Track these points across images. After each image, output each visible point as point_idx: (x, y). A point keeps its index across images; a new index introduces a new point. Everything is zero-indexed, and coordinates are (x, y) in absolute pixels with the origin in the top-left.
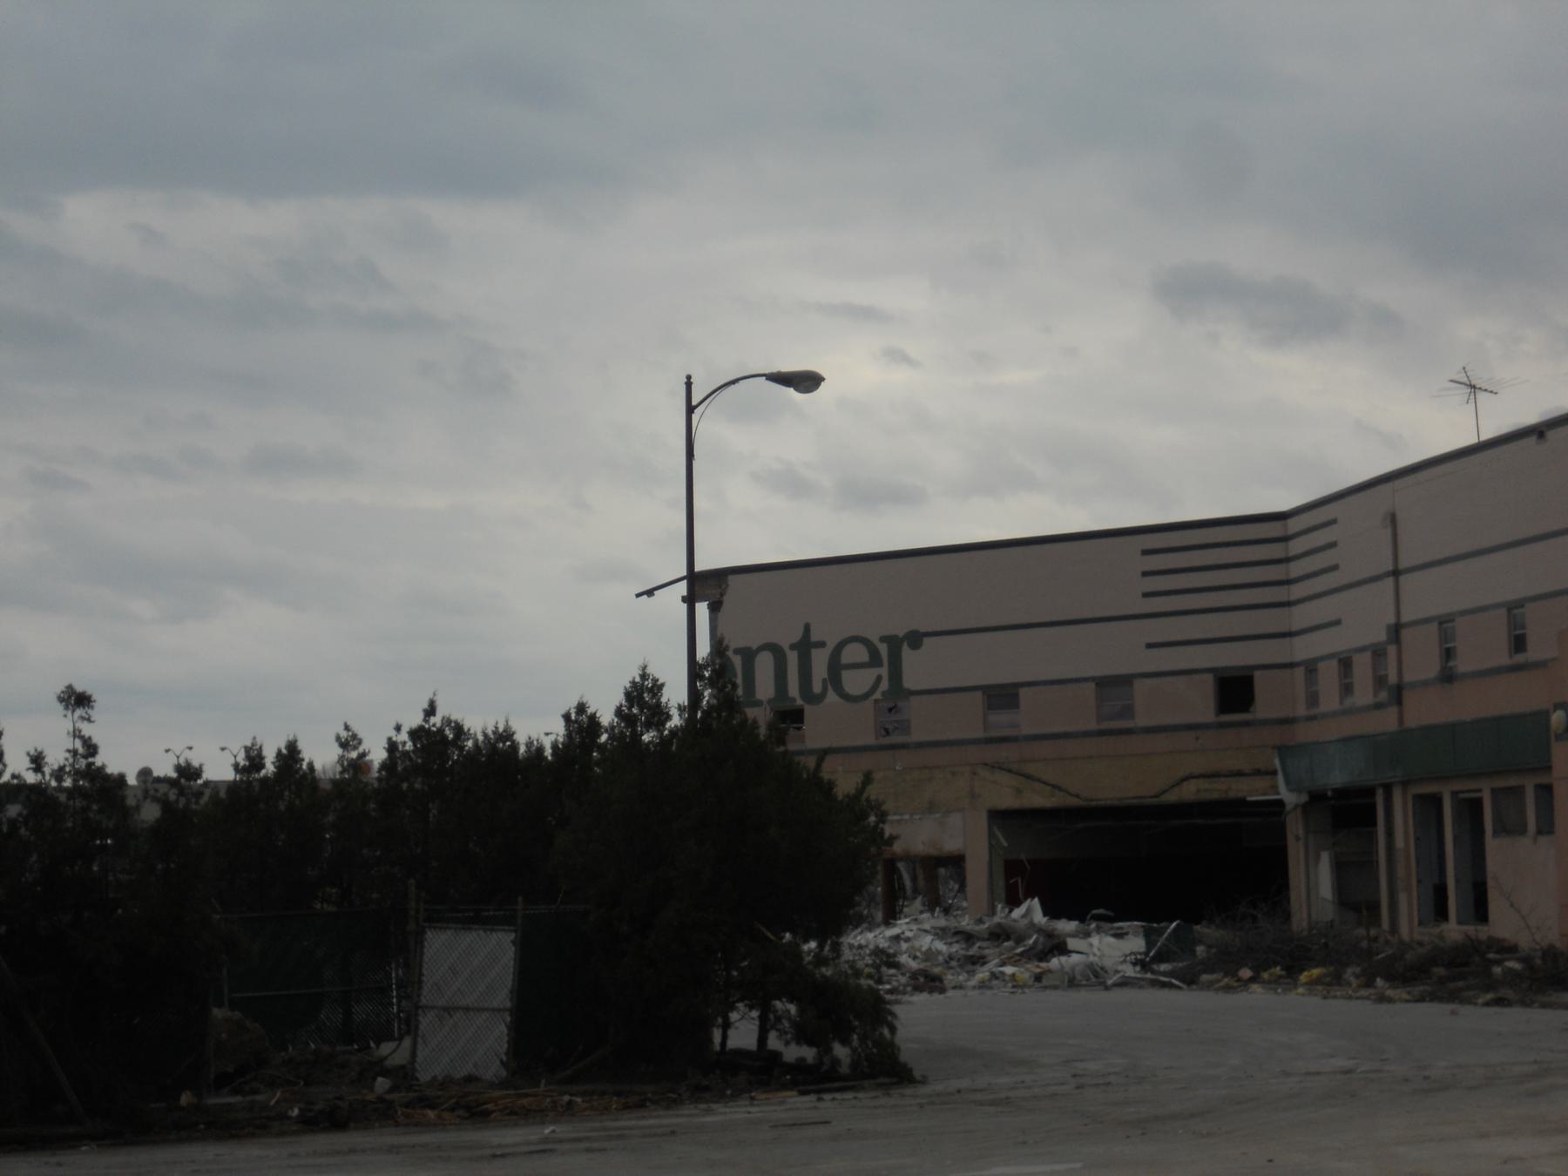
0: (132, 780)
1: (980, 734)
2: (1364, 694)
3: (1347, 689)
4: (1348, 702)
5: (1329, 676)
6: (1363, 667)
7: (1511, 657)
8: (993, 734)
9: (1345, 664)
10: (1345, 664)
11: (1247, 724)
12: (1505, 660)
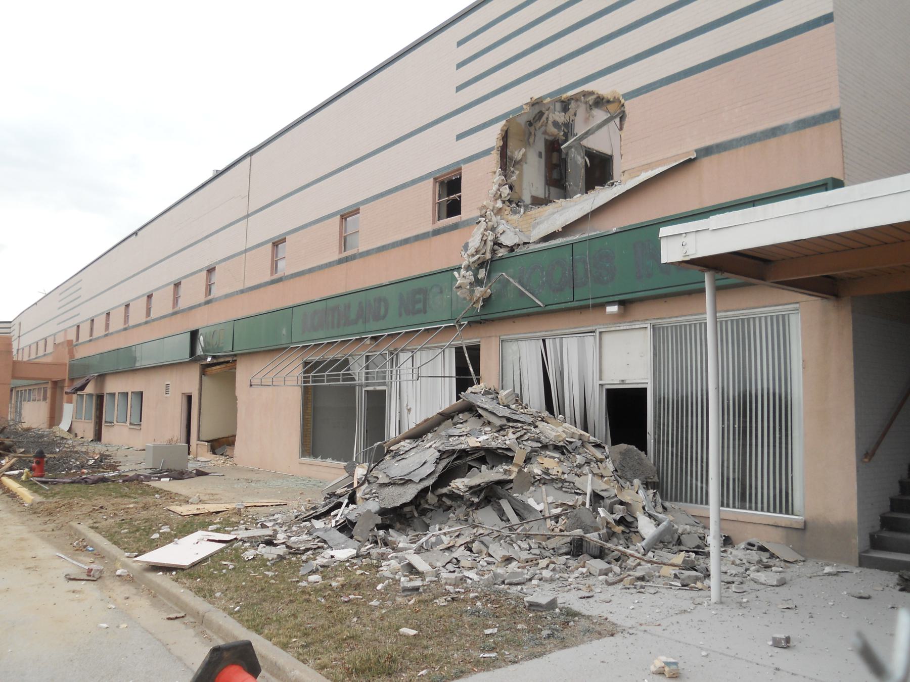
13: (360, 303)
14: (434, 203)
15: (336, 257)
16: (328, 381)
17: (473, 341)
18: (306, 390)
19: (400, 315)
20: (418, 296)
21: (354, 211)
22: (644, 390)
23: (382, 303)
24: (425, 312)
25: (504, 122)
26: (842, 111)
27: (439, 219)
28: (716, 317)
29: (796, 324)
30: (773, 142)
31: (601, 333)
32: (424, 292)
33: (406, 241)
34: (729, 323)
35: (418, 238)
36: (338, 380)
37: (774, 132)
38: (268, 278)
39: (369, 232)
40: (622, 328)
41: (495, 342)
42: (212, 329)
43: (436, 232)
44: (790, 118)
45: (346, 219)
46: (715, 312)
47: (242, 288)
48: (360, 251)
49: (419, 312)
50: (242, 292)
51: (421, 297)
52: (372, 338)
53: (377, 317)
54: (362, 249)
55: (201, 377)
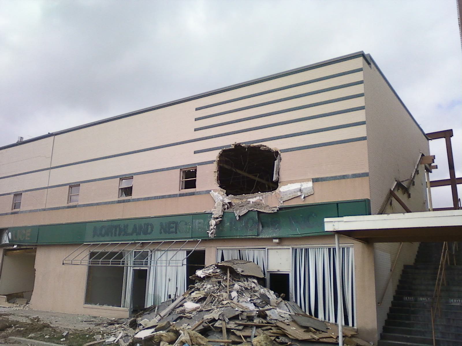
0: (143, 225)
13: (135, 225)
14: (180, 181)
15: (10, 211)
16: (112, 264)
17: (306, 246)
18: (90, 268)
19: (161, 233)
20: (172, 225)
21: (77, 185)
22: (288, 274)
23: (150, 226)
24: (176, 233)
25: (221, 150)
26: (370, 174)
27: (14, 209)
28: (339, 246)
29: (351, 250)
30: (343, 181)
31: (268, 249)
32: (176, 223)
33: (163, 197)
34: (300, 249)
35: (170, 196)
36: (109, 264)
37: (344, 177)
38: (66, 205)
39: (84, 196)
40: (278, 248)
41: (213, 250)
42: (110, 223)
43: (181, 195)
44: (350, 173)
45: (72, 188)
46: (339, 244)
47: (44, 207)
48: (79, 204)
49: (172, 232)
50: (44, 210)
51: (174, 225)
52: (142, 243)
53: (146, 233)
54: (80, 203)
55: (3, 256)
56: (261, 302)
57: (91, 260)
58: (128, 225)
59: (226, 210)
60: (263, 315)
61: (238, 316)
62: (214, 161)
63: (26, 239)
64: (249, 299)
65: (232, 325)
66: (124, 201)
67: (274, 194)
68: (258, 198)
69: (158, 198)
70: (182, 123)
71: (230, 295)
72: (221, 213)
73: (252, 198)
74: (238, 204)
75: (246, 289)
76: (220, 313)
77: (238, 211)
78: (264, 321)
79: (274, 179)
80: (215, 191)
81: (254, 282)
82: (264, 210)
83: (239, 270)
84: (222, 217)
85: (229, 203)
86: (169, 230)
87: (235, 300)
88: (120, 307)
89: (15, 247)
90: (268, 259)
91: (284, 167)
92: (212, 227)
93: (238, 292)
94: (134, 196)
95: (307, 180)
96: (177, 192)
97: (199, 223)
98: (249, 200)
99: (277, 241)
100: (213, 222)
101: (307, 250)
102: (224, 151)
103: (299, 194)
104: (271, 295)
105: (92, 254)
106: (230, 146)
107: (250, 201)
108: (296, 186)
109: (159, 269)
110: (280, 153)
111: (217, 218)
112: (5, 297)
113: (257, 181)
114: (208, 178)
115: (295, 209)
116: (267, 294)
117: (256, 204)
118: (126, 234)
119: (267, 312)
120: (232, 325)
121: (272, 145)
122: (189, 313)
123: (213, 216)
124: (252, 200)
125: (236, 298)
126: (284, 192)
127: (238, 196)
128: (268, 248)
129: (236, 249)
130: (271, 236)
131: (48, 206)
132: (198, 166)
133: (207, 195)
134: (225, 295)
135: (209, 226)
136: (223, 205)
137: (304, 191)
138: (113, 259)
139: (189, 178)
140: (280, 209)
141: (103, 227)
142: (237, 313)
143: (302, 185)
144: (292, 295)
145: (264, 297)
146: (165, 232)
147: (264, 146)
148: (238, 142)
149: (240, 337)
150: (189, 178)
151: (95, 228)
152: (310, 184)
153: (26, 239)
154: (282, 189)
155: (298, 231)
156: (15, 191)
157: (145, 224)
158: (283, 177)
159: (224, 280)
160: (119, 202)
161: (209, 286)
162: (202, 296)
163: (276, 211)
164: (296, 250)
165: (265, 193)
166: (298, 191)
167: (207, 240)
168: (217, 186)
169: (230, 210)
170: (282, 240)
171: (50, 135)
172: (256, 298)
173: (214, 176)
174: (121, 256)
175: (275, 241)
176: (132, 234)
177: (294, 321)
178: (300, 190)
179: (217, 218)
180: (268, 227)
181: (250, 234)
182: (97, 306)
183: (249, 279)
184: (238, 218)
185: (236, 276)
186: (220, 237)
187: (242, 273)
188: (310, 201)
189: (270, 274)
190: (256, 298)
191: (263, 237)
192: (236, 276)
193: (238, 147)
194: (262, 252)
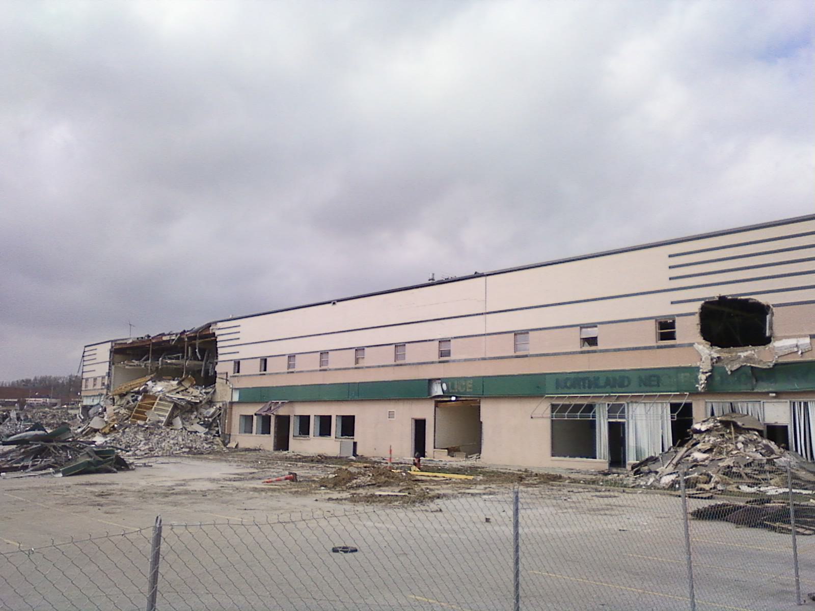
0: (618, 378)
1: (512, 353)
2: (99, 386)
3: (95, 385)
4: (95, 388)
5: (91, 382)
6: (99, 381)
7: (657, 342)
8: (518, 353)
9: (95, 379)
10: (95, 379)
11: (673, 346)
12: (354, 366)
17: (805, 400)
20: (653, 378)
24: (659, 386)
25: (703, 302)
32: (658, 377)
47: (483, 356)
50: (484, 359)
51: (655, 378)
53: (621, 386)
54: (531, 353)
56: (767, 451)
57: (554, 414)
58: (599, 378)
59: (715, 365)
60: (770, 462)
61: (750, 463)
62: (697, 313)
63: (468, 390)
64: (754, 450)
65: (748, 470)
66: (588, 352)
67: (767, 348)
68: (749, 352)
69: (629, 348)
70: (654, 268)
71: (736, 447)
72: (710, 368)
73: (742, 352)
74: (727, 358)
75: (751, 440)
76: (733, 461)
77: (729, 366)
78: (774, 468)
79: (768, 334)
80: (699, 343)
81: (755, 434)
82: (759, 364)
83: (739, 424)
84: (711, 371)
85: (718, 357)
86: (649, 383)
87: (742, 450)
88: (596, 458)
89: (453, 398)
90: (763, 410)
91: (777, 322)
92: (702, 382)
93: (743, 443)
94: (601, 346)
95: (805, 336)
96: (654, 344)
97: (685, 377)
98: (739, 354)
99: (774, 395)
100: (702, 377)
101: (806, 404)
102: (706, 303)
103: (796, 349)
104: (772, 445)
105: (554, 407)
106: (714, 297)
107: (740, 356)
108: (793, 342)
109: (639, 423)
110: (772, 307)
111: (706, 373)
112: (446, 450)
113: (661, 329)
114: (689, 330)
115: (789, 366)
116: (769, 444)
117: (748, 359)
118: (597, 386)
119: (775, 460)
120: (748, 470)
121: (762, 299)
122: (702, 461)
123: (701, 370)
124: (743, 355)
125: (743, 448)
126: (778, 347)
127: (726, 350)
128: (765, 401)
129: (728, 402)
130: (766, 390)
131: (488, 355)
132: (676, 318)
133: (691, 348)
134: (732, 447)
135: (697, 381)
136: (712, 359)
137: (801, 347)
138: (581, 412)
139: (666, 329)
140: (776, 365)
141: (567, 379)
142: (749, 461)
143: (798, 341)
144: (792, 445)
145: (767, 447)
146: (645, 385)
147: (752, 299)
148: (722, 294)
149: (758, 479)
150: (666, 329)
151: (557, 380)
152: (807, 340)
153: (468, 390)
154: (776, 344)
155: (796, 386)
156: (439, 337)
157: (620, 377)
158: (777, 332)
159: (727, 433)
160: (582, 352)
161: (712, 439)
162: (709, 448)
163: (771, 367)
164: (794, 403)
165: (757, 347)
166: (794, 347)
167: (695, 393)
168: (701, 339)
169: (719, 364)
170: (779, 394)
171: (477, 275)
172: (760, 448)
173: (697, 329)
174: (590, 408)
175: (771, 395)
176: (605, 387)
177: (801, 467)
178: (797, 346)
179: (706, 373)
180: (763, 381)
181: (743, 388)
182: (568, 458)
183: (750, 432)
184: (729, 373)
185: (739, 430)
186: (712, 389)
187: (744, 427)
188: (808, 358)
189: (767, 426)
190: (760, 448)
191: (759, 391)
192: (739, 430)
193: (722, 299)
194: (757, 405)
